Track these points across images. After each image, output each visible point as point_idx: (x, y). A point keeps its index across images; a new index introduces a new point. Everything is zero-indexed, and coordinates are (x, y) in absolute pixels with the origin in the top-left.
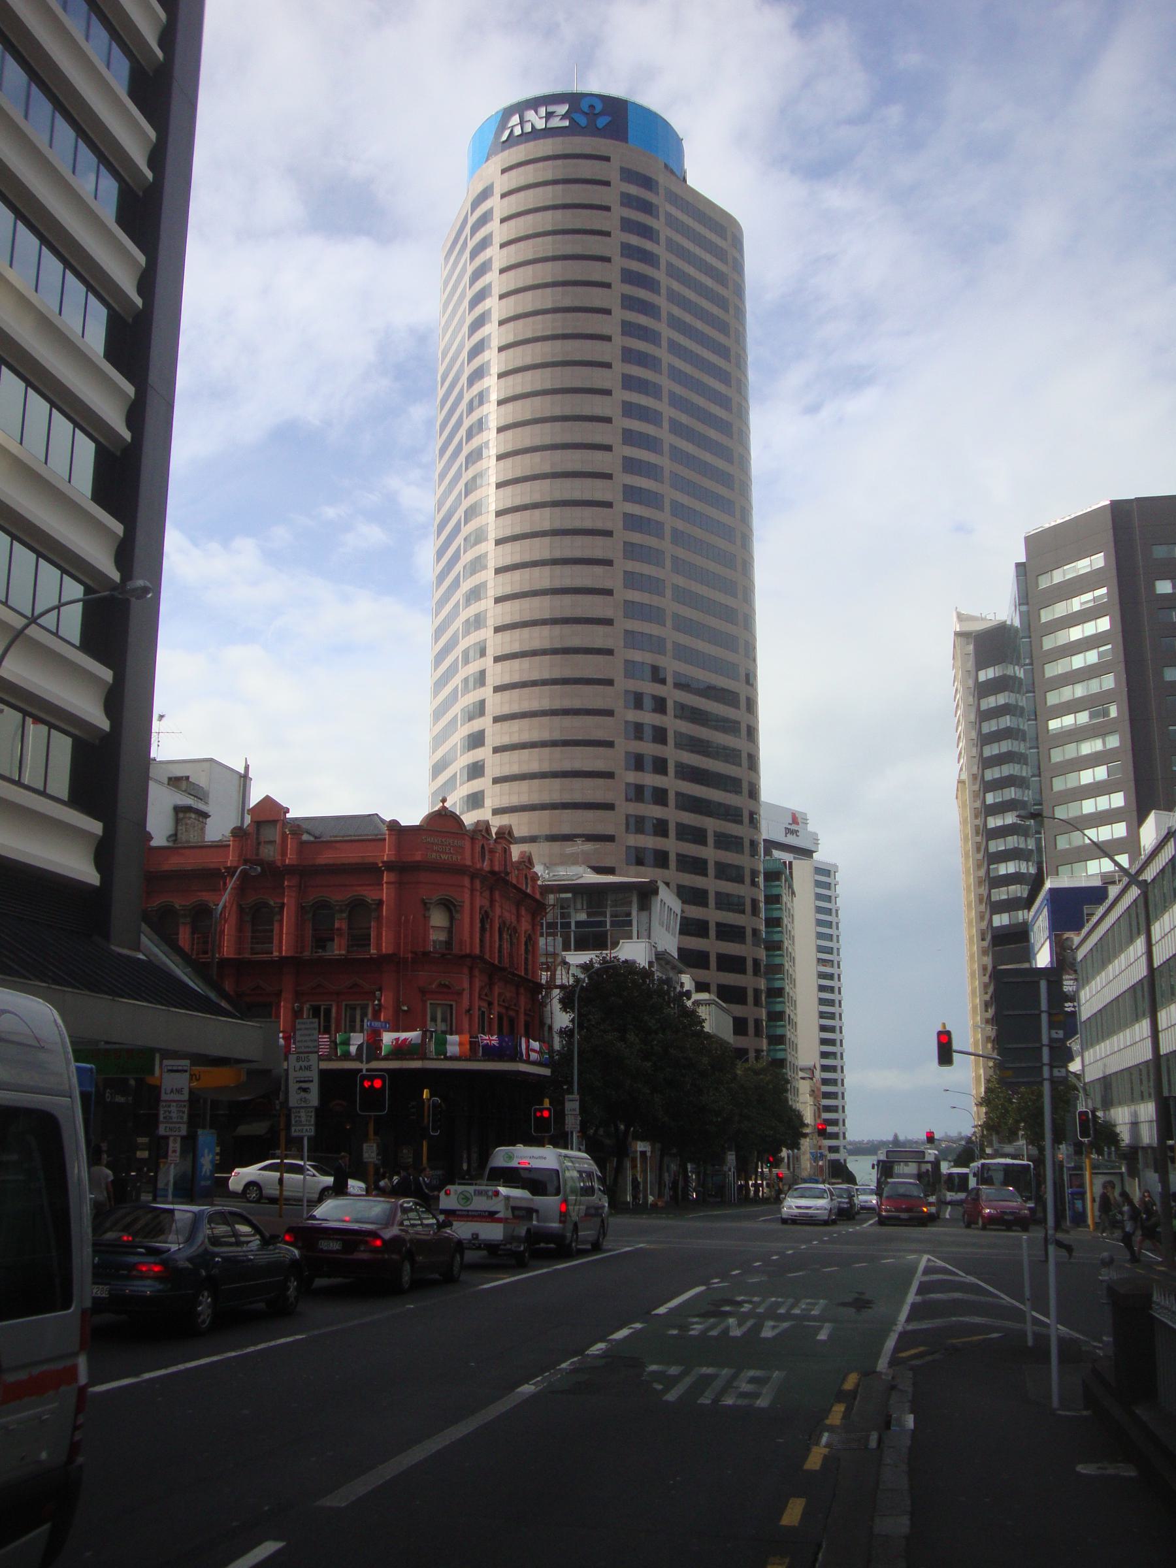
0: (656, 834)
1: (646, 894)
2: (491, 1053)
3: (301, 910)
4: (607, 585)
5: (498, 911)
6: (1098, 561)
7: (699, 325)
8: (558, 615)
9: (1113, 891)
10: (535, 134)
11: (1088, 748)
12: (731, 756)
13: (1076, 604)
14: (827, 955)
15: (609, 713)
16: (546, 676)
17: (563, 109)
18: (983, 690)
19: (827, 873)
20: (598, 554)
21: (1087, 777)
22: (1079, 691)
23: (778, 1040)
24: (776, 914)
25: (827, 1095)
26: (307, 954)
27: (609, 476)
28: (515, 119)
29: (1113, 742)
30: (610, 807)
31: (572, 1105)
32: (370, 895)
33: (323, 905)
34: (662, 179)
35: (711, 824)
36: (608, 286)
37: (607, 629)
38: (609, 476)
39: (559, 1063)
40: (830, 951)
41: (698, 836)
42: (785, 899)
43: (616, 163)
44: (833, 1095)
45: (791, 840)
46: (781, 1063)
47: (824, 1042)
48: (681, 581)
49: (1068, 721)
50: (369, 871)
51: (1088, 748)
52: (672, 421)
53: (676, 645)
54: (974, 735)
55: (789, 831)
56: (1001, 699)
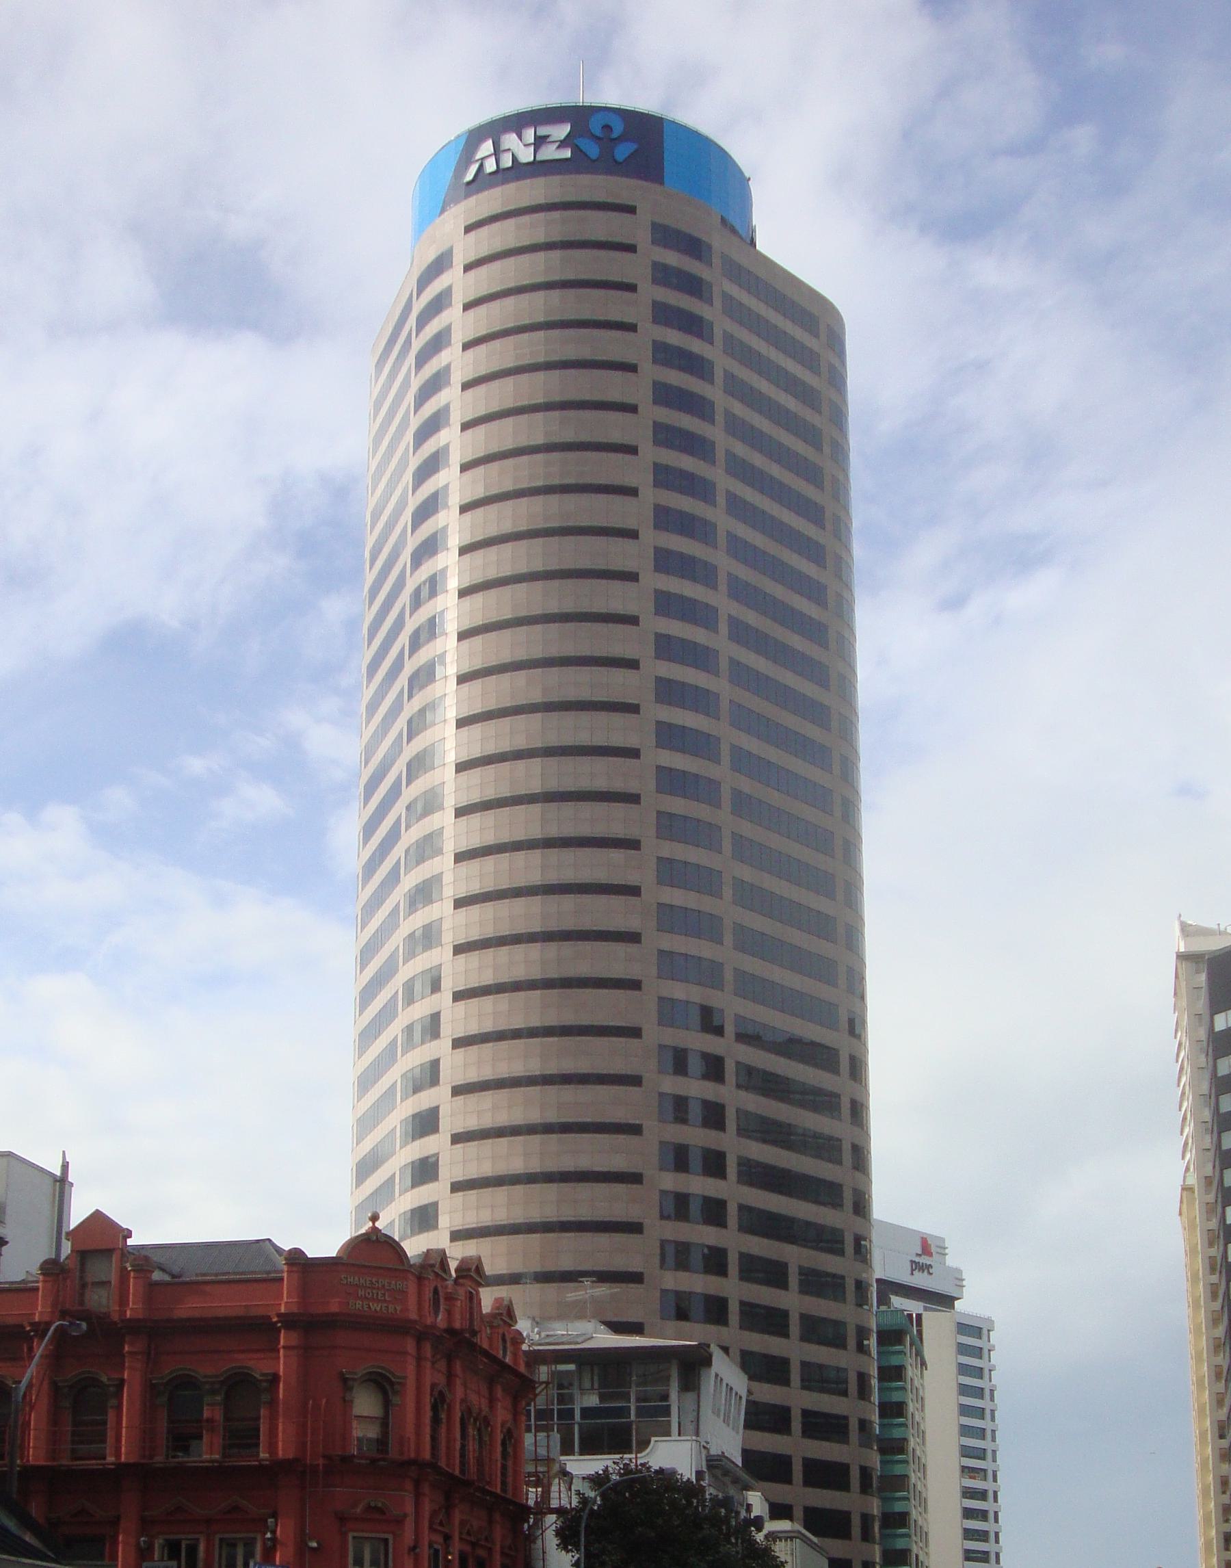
0: (708, 1270)
1: (692, 1365)
3: (151, 1389)
4: (632, 879)
5: (459, 1392)
7: (775, 470)
8: (553, 926)
10: (518, 171)
15: (635, 1081)
17: (561, 131)
19: (976, 1332)
24: (896, 1397)
26: (159, 1459)
27: (633, 709)
28: (487, 147)
32: (259, 1366)
33: (185, 1382)
34: (718, 241)
35: (794, 1256)
37: (632, 948)
38: (633, 709)
41: (774, 1274)
42: (910, 1372)
43: (645, 216)
45: (919, 1280)
48: (747, 873)
50: (258, 1329)
53: (740, 974)
55: (916, 1267)
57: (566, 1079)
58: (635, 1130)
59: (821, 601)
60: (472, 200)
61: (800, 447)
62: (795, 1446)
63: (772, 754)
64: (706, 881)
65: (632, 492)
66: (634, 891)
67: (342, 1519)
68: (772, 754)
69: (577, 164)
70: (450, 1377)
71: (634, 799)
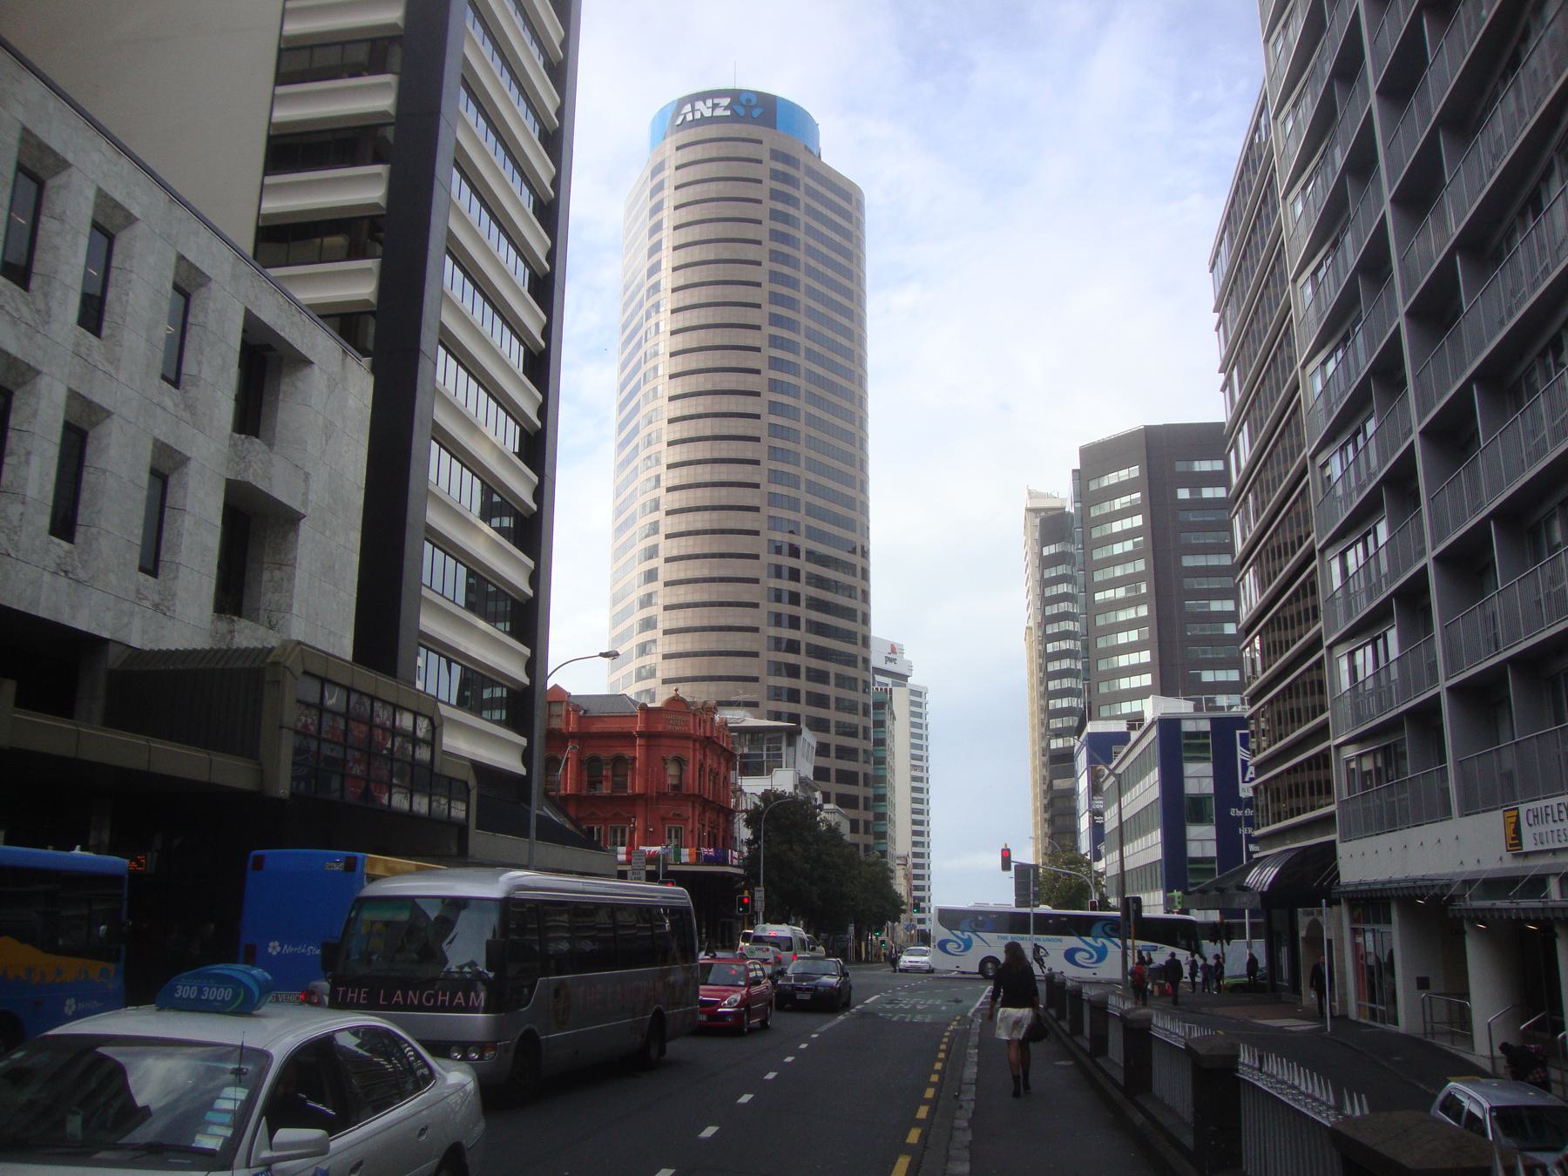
0: (789, 675)
1: (792, 735)
2: (709, 860)
3: (580, 762)
4: (756, 479)
5: (709, 761)
6: (1134, 472)
7: (829, 272)
8: (716, 503)
9: (1134, 735)
10: (704, 121)
11: (1124, 615)
12: (849, 614)
13: (1118, 504)
14: (918, 759)
15: (756, 581)
16: (706, 551)
17: (726, 101)
18: (1046, 562)
19: (919, 694)
20: (749, 456)
21: (1123, 638)
22: (1118, 571)
23: (882, 835)
24: (880, 736)
25: (917, 877)
26: (584, 792)
27: (757, 394)
28: (688, 108)
29: (1143, 611)
30: (755, 655)
31: (760, 894)
32: (627, 753)
33: (595, 760)
34: (803, 158)
35: (833, 668)
36: (759, 243)
37: (754, 514)
38: (757, 394)
39: (750, 863)
40: (920, 758)
41: (820, 676)
42: (888, 723)
43: (766, 147)
44: (921, 877)
45: (890, 667)
46: (883, 854)
47: (915, 833)
48: (812, 477)
49: (1110, 594)
50: (627, 737)
51: (1124, 615)
52: (808, 350)
53: (808, 528)
54: (1038, 576)
55: (889, 660)
56: (1061, 570)
57: (722, 580)
58: (756, 605)
59: (851, 298)
60: (680, 134)
61: (839, 220)
62: (833, 763)
63: (826, 416)
64: (794, 482)
65: (759, 285)
66: (756, 486)
67: (663, 819)
68: (826, 416)
69: (734, 118)
70: (705, 756)
71: (757, 439)
